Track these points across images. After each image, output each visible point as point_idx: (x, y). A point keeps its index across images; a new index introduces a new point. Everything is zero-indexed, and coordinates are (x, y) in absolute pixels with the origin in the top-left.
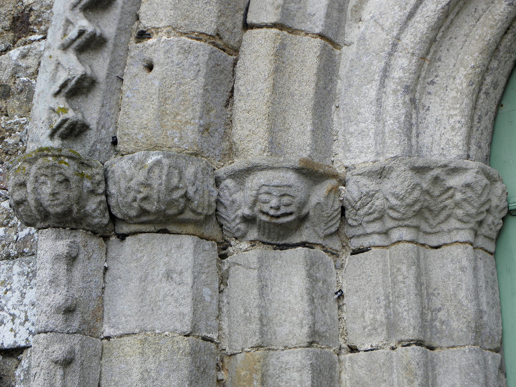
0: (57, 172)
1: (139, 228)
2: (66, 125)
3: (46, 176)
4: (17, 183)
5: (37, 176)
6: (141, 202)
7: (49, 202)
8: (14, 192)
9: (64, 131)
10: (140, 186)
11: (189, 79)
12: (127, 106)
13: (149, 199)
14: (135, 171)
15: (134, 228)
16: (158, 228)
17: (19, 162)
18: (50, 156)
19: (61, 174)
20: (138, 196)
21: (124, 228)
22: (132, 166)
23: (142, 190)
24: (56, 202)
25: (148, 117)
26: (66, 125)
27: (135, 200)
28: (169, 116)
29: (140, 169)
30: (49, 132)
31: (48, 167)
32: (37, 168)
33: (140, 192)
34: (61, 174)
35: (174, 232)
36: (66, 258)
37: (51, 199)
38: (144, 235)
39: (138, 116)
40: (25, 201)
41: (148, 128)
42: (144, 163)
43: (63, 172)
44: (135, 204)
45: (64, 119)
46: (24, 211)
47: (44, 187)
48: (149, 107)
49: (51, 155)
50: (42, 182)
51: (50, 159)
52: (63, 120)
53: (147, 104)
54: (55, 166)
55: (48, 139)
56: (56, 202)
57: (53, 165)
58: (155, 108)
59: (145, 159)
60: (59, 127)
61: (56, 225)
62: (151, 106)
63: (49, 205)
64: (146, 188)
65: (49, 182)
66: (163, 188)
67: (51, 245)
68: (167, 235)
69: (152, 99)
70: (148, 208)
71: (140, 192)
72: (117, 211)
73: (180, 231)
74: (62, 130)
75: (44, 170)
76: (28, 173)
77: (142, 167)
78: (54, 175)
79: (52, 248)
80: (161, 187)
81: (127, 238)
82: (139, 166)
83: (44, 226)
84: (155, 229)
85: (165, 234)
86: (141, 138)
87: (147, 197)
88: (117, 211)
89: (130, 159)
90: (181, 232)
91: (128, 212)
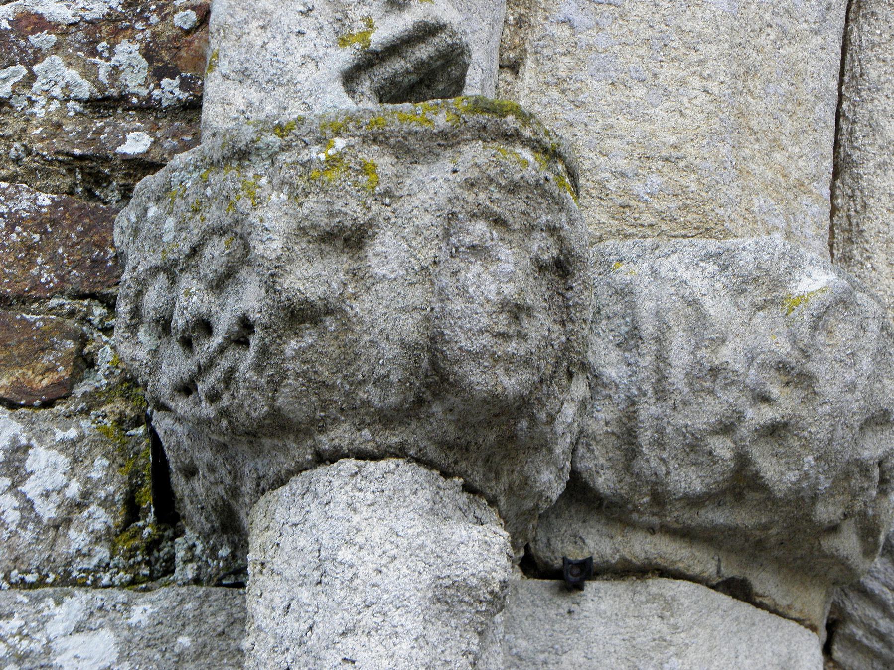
0: (544, 219)
1: (669, 550)
2: (423, 52)
3: (498, 222)
4: (314, 227)
5: (453, 214)
6: (754, 442)
7: (486, 340)
8: (290, 260)
9: (408, 72)
10: (772, 372)
11: (805, 26)
12: (567, 59)
13: (785, 438)
14: (733, 309)
15: (647, 547)
16: (730, 571)
17: (338, 134)
18: (526, 143)
19: (553, 230)
20: (750, 413)
21: (590, 542)
22: (718, 286)
23: (775, 391)
24: (512, 347)
25: (681, 120)
26: (423, 52)
27: (726, 428)
28: (757, 140)
29: (761, 308)
30: (345, 57)
31: (513, 188)
32: (459, 178)
33: (765, 399)
34: (553, 230)
35: (766, 601)
36: (491, 603)
37: (501, 328)
38: (684, 586)
39: (623, 109)
40: (329, 312)
41: (682, 164)
42: (784, 287)
43: (561, 228)
44: (723, 448)
45: (428, 19)
46: (310, 355)
47: (473, 271)
48: (683, 83)
49: (530, 140)
50: (473, 247)
51: (526, 154)
52: (426, 24)
53: (668, 72)
54: (545, 194)
55: (338, 87)
56: (512, 347)
57: (538, 185)
58: (716, 90)
59: (789, 271)
60: (394, 49)
61: (432, 452)
62: (696, 82)
63: (477, 356)
64: (787, 390)
65: (505, 252)
66: (855, 406)
67: (419, 535)
68: (745, 609)
69: (694, 57)
70: (769, 475)
71: (765, 399)
72: (602, 461)
73: (783, 602)
74: (397, 65)
75: (496, 195)
76: (387, 193)
77: (773, 302)
78: (530, 229)
79: (422, 547)
80: (849, 396)
81: (591, 586)
82: (758, 295)
83: (370, 446)
84: (718, 572)
85: (742, 603)
86: (651, 194)
87: (786, 425)
88: (602, 461)
89: (708, 256)
90: (789, 607)
91: (668, 473)
